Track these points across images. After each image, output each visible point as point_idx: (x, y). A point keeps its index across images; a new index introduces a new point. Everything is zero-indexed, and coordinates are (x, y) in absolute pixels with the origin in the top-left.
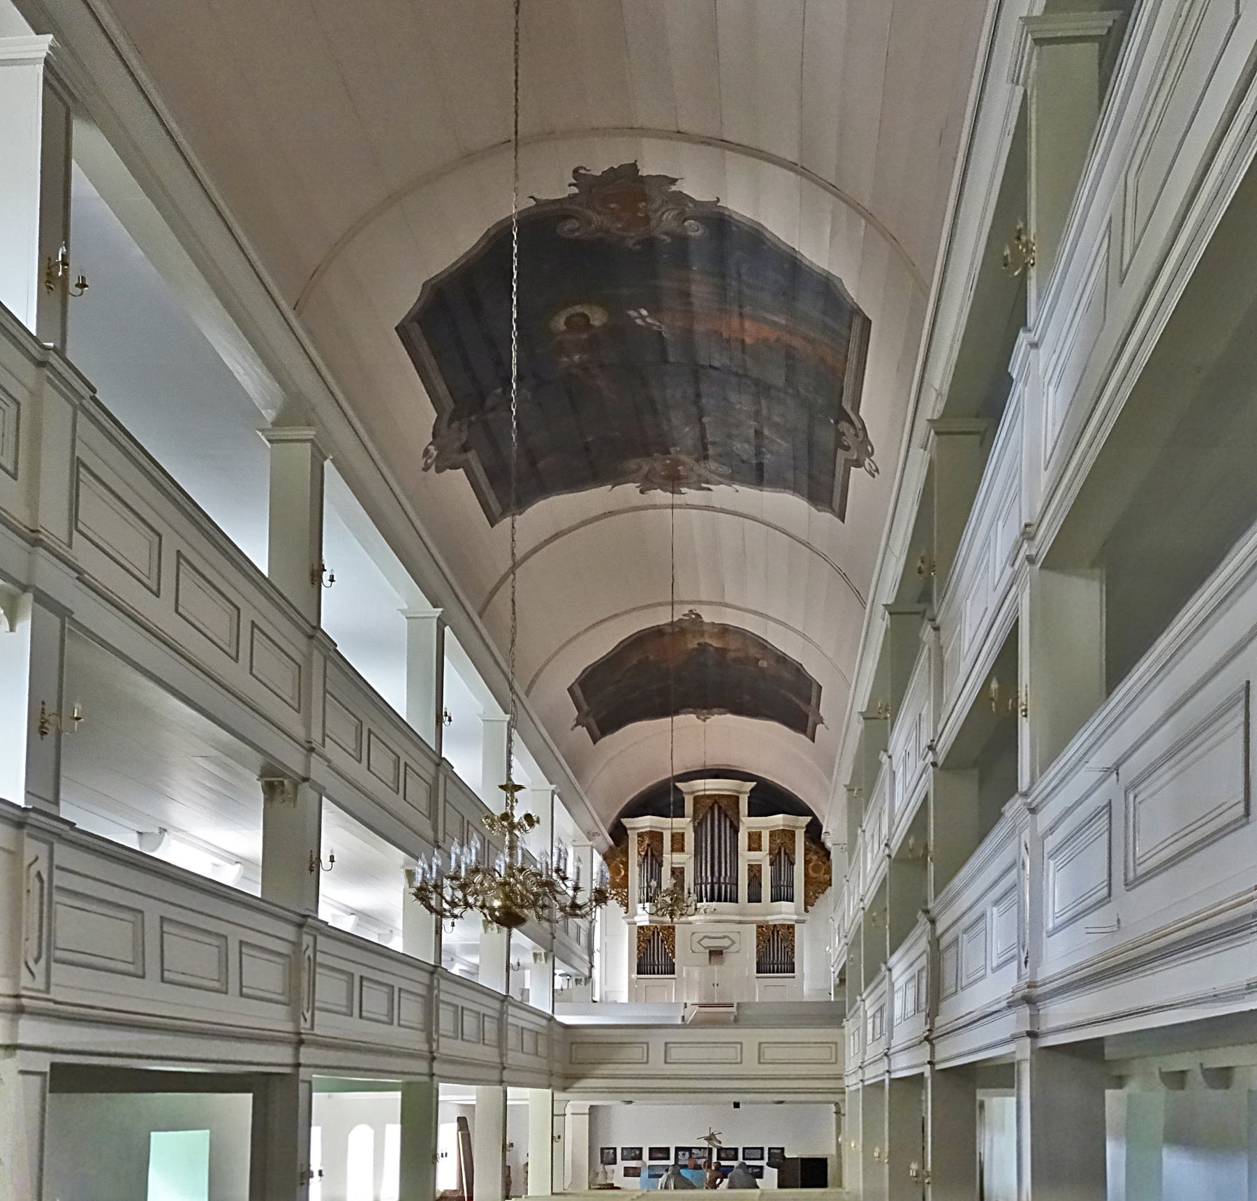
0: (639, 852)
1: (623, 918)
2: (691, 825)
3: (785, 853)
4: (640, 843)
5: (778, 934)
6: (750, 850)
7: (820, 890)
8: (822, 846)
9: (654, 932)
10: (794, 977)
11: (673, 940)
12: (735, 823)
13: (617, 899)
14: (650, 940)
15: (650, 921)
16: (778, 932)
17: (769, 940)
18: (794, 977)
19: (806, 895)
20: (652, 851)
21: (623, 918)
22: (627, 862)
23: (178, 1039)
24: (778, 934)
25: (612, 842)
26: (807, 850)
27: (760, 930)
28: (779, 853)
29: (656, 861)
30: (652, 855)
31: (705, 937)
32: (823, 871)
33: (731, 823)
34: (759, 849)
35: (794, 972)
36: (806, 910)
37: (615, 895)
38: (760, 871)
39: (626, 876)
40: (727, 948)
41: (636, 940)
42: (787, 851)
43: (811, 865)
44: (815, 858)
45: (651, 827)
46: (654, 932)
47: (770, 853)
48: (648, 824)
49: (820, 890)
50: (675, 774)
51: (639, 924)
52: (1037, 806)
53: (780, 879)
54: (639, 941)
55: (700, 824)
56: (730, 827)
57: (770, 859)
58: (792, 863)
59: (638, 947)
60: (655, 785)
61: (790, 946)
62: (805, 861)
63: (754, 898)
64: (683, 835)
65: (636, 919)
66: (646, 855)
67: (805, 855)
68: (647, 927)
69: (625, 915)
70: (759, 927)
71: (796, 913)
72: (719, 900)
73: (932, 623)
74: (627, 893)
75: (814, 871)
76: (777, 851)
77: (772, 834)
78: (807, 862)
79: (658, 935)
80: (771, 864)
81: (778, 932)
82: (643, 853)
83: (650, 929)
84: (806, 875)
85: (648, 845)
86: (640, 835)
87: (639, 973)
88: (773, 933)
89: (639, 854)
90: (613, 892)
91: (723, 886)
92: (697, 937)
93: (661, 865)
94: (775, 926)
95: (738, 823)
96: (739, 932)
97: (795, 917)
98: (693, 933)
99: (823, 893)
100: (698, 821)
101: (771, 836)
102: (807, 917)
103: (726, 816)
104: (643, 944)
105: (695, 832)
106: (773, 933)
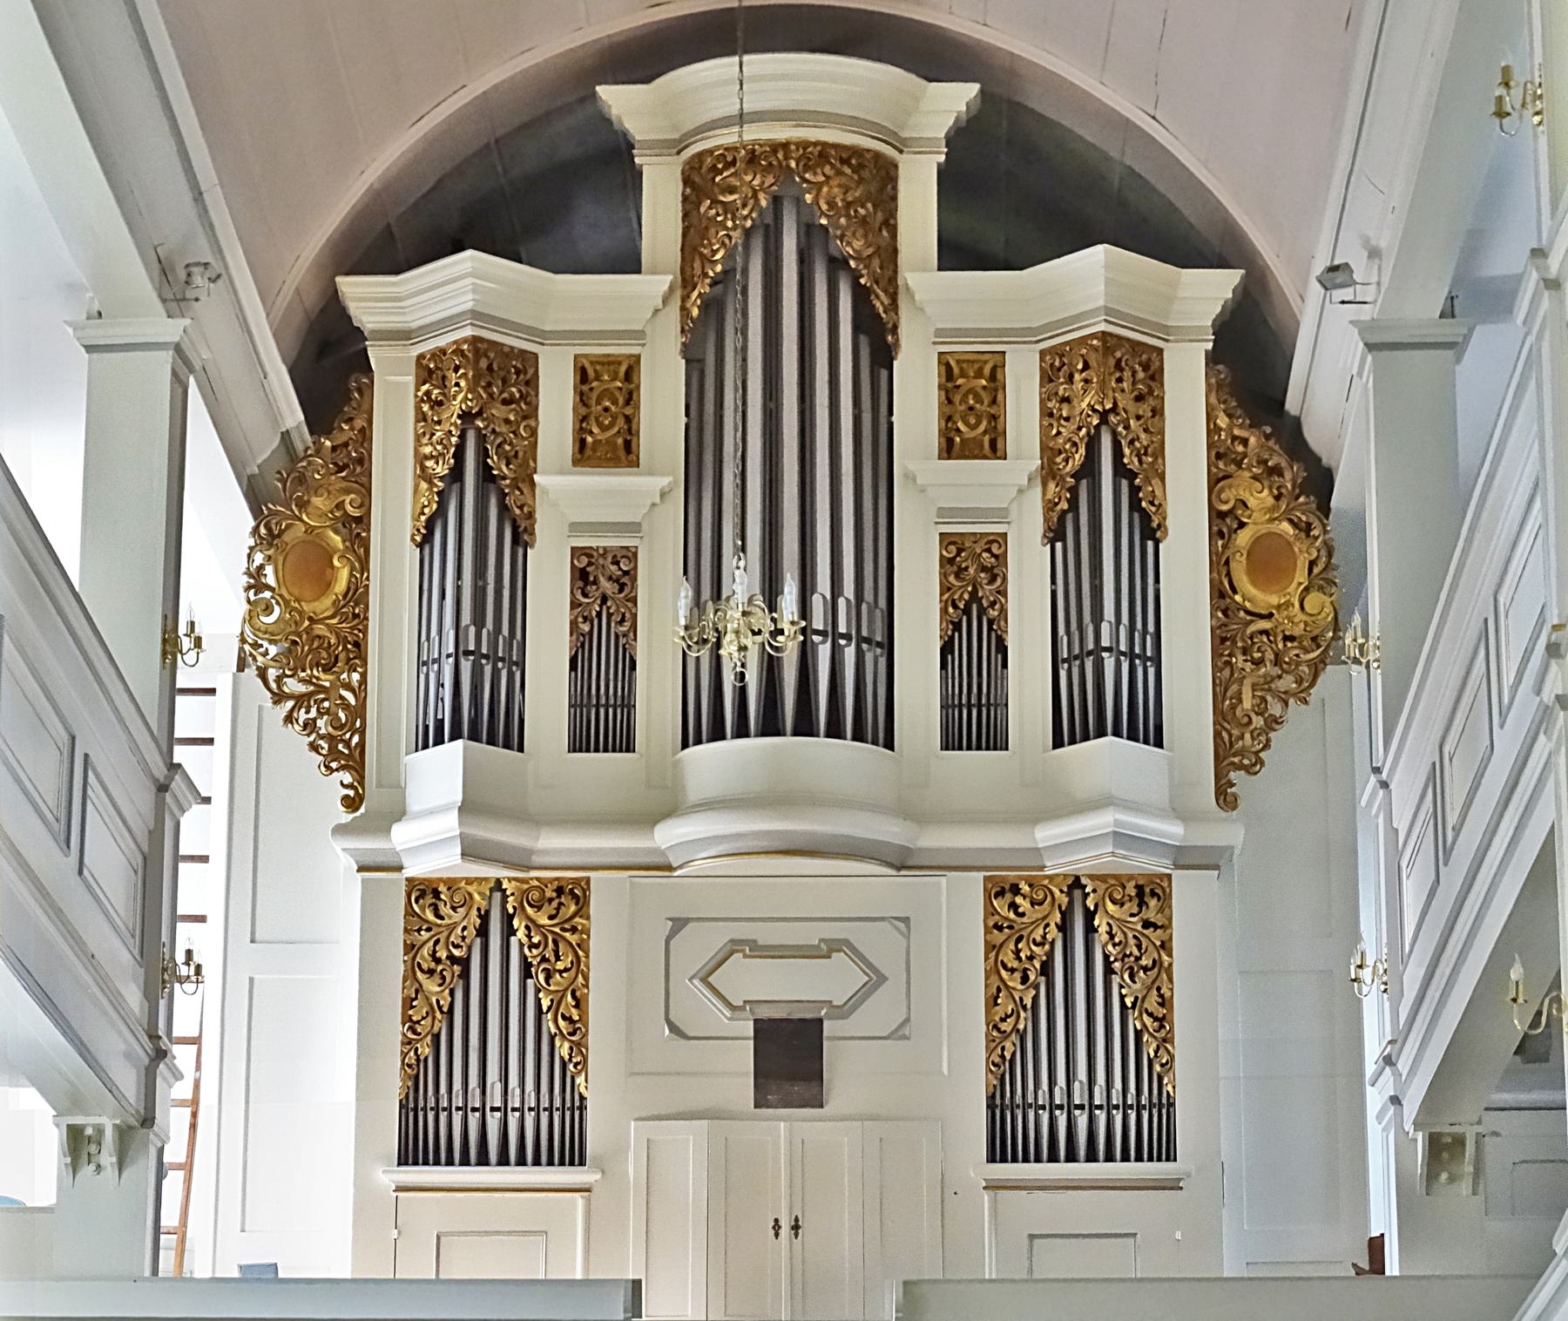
0: (421, 459)
1: (340, 830)
2: (673, 313)
3: (1120, 470)
4: (429, 409)
5: (1090, 929)
6: (949, 449)
7: (1288, 683)
8: (1291, 436)
9: (485, 918)
10: (1173, 1185)
11: (578, 966)
12: (880, 303)
13: (310, 726)
14: (465, 963)
15: (471, 851)
16: (1089, 916)
17: (1046, 969)
18: (1173, 1185)
19: (1223, 715)
20: (483, 454)
21: (340, 830)
22: (363, 521)
23: (264, 737)
24: (1090, 929)
25: (293, 415)
26: (1223, 460)
27: (1000, 905)
28: (1090, 470)
29: (504, 509)
30: (486, 475)
31: (735, 947)
32: (1301, 576)
33: (861, 296)
34: (996, 449)
35: (1171, 1157)
36: (1225, 796)
37: (301, 700)
38: (996, 572)
39: (357, 595)
40: (843, 1012)
41: (397, 963)
42: (1130, 460)
43: (1243, 538)
44: (1259, 498)
45: (476, 316)
46: (485, 918)
47: (1049, 472)
48: (466, 302)
49: (1288, 683)
50: (736, 59)
51: (417, 868)
52: (1559, 271)
53: (1098, 617)
54: (412, 968)
55: (713, 308)
56: (857, 329)
57: (1049, 506)
58: (1150, 530)
59: (408, 1003)
60: (1243, 231)
61: (1152, 1003)
62: (1216, 515)
63: (465, 1162)
64: (631, 371)
65: (402, 835)
66: (457, 474)
67: (1215, 481)
68: (451, 884)
69: (347, 818)
70: (1002, 889)
71: (1178, 812)
72: (805, 727)
73: (1378, 775)
74: (361, 690)
75: (1254, 572)
76: (1079, 457)
77: (1055, 368)
78: (1223, 522)
79: (509, 931)
80: (1055, 534)
81: (1089, 916)
82: (442, 469)
83: (468, 901)
84: (1221, 594)
85: (466, 416)
86: (430, 371)
87: (406, 1157)
88: (1065, 928)
89: (424, 475)
90: (293, 686)
91: (824, 652)
92: (698, 947)
93: (522, 537)
94: (1076, 883)
95: (894, 306)
96: (906, 920)
97: (1173, 831)
98: (679, 924)
99: (1302, 697)
100: (704, 288)
101: (1047, 377)
102: (1228, 832)
103: (837, 264)
104: (431, 986)
105: (693, 362)
106: (1065, 928)
